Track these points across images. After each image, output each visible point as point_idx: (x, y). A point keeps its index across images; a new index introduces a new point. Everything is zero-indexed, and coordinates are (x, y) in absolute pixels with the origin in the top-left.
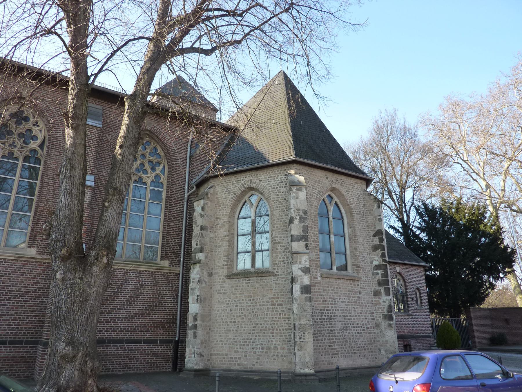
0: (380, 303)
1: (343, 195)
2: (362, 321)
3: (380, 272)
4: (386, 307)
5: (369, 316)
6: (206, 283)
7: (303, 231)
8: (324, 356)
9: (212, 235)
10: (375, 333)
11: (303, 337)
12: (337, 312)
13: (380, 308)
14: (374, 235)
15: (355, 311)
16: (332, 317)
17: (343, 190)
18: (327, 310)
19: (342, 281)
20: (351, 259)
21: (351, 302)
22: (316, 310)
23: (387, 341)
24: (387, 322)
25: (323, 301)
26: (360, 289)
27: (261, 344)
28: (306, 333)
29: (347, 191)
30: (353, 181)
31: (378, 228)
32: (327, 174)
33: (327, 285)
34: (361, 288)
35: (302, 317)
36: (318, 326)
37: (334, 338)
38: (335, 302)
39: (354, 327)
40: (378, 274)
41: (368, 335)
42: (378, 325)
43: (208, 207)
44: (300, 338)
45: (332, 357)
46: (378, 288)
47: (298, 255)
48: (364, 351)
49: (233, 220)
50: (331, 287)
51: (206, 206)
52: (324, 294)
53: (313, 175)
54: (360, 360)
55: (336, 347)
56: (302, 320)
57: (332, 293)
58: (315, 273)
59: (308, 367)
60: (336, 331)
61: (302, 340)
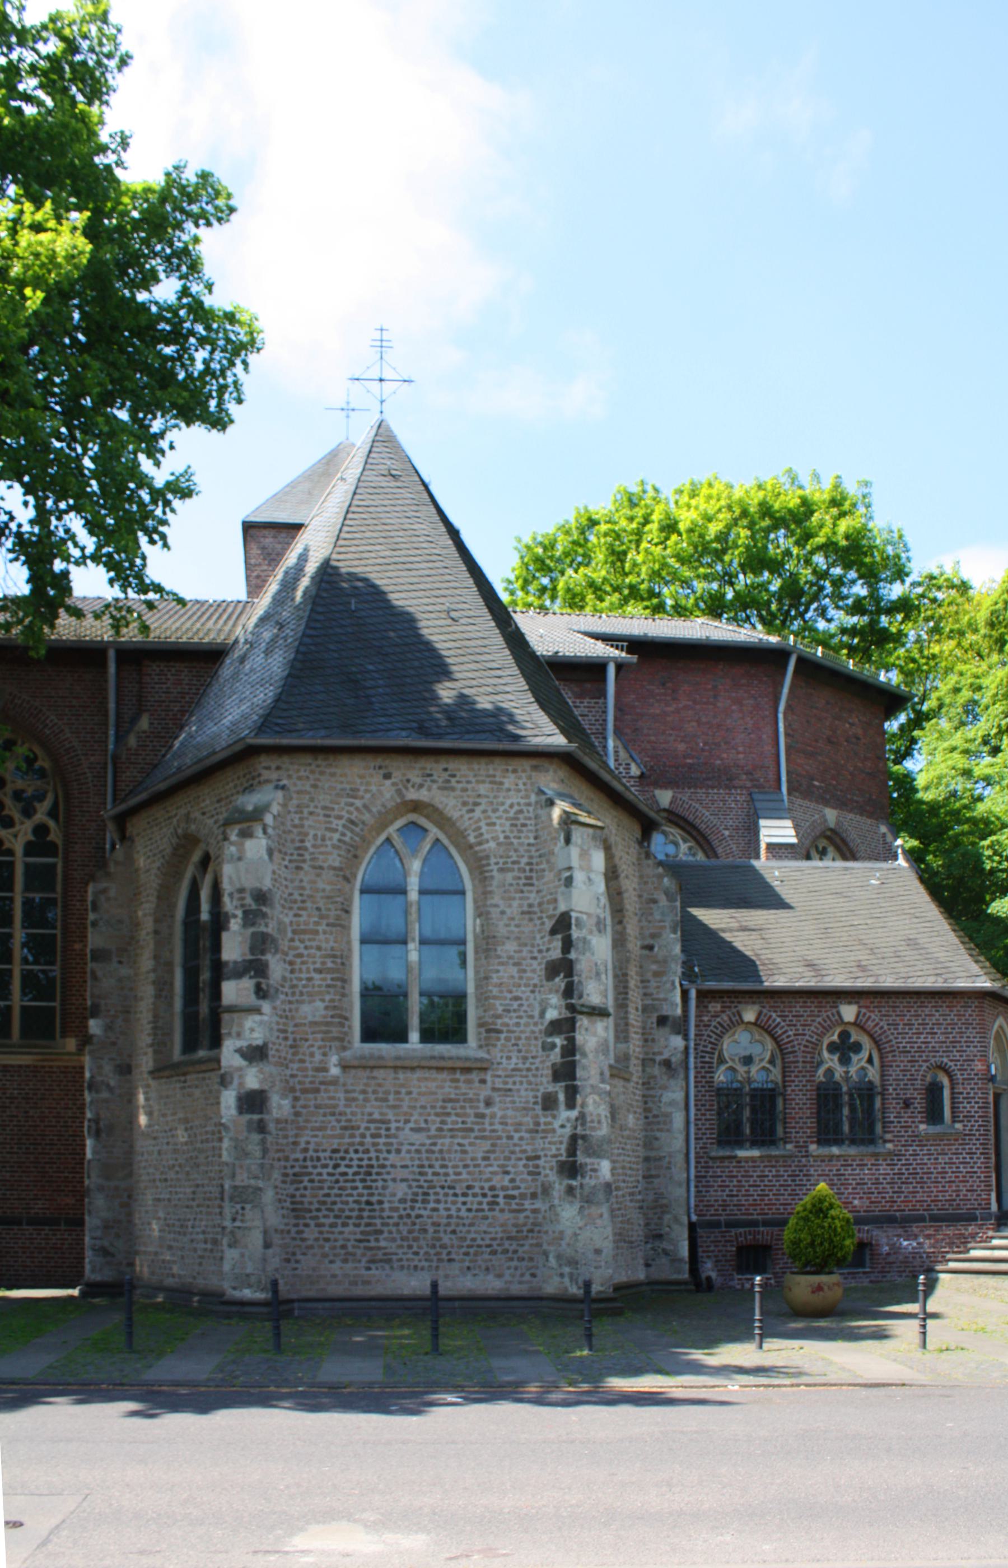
0: (554, 1131)
1: (449, 819)
2: (489, 1180)
3: (559, 1041)
4: (566, 1140)
5: (519, 1167)
6: (110, 1088)
7: (253, 949)
8: (338, 1264)
9: (124, 971)
10: (535, 1211)
11: (239, 1217)
12: (392, 1157)
13: (554, 1143)
14: (553, 932)
15: (464, 1152)
16: (374, 1171)
17: (450, 804)
18: (356, 1151)
19: (418, 1074)
20: (477, 1007)
21: (451, 1130)
22: (316, 1151)
23: (562, 1232)
24: (567, 1182)
25: (345, 1128)
26: (489, 1092)
27: (204, 1232)
28: (248, 1206)
29: (465, 804)
30: (496, 768)
31: (562, 908)
32: (387, 762)
33: (362, 1087)
34: (494, 1089)
35: (238, 1171)
36: (322, 1192)
37: (378, 1221)
38: (388, 1129)
39: (455, 1195)
40: (553, 1046)
41: (507, 1215)
42: (546, 1190)
43: (108, 899)
44: (234, 1220)
45: (369, 1269)
46: (551, 1088)
47: (235, 1015)
48: (486, 1256)
49: (171, 927)
50: (374, 1092)
51: (102, 898)
52: (348, 1111)
53: (333, 775)
54: (469, 1277)
55: (383, 1244)
56: (238, 1178)
57: (380, 1107)
58: (318, 1057)
59: (250, 1286)
60: (386, 1205)
61: (238, 1224)
